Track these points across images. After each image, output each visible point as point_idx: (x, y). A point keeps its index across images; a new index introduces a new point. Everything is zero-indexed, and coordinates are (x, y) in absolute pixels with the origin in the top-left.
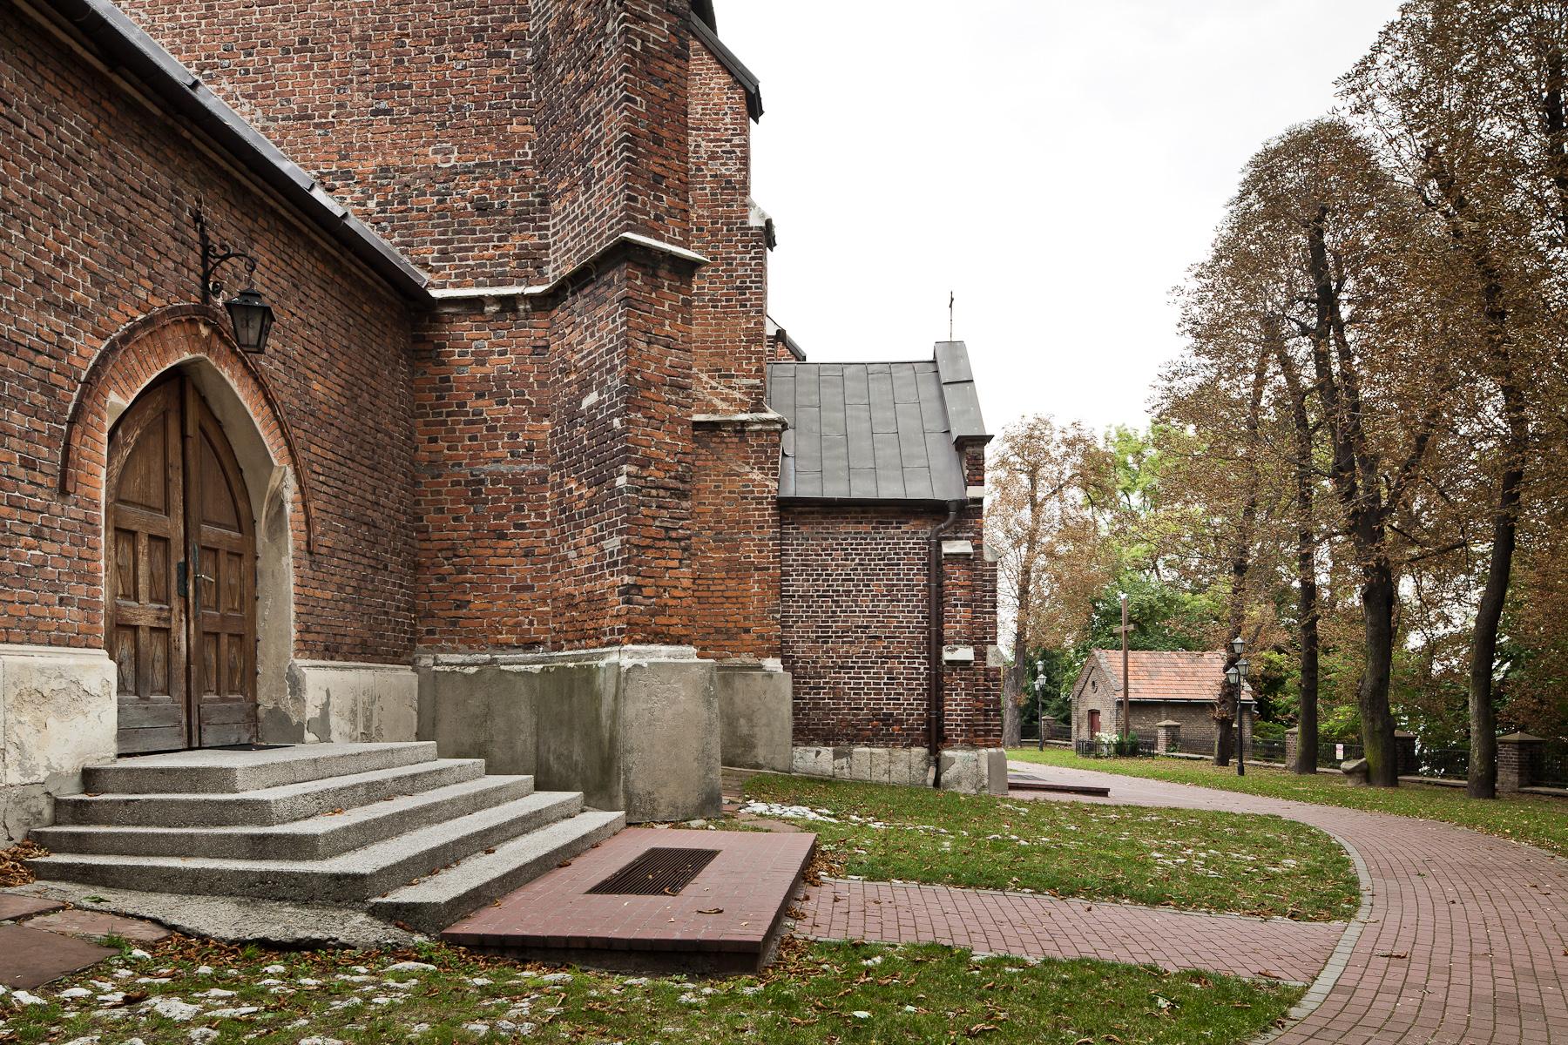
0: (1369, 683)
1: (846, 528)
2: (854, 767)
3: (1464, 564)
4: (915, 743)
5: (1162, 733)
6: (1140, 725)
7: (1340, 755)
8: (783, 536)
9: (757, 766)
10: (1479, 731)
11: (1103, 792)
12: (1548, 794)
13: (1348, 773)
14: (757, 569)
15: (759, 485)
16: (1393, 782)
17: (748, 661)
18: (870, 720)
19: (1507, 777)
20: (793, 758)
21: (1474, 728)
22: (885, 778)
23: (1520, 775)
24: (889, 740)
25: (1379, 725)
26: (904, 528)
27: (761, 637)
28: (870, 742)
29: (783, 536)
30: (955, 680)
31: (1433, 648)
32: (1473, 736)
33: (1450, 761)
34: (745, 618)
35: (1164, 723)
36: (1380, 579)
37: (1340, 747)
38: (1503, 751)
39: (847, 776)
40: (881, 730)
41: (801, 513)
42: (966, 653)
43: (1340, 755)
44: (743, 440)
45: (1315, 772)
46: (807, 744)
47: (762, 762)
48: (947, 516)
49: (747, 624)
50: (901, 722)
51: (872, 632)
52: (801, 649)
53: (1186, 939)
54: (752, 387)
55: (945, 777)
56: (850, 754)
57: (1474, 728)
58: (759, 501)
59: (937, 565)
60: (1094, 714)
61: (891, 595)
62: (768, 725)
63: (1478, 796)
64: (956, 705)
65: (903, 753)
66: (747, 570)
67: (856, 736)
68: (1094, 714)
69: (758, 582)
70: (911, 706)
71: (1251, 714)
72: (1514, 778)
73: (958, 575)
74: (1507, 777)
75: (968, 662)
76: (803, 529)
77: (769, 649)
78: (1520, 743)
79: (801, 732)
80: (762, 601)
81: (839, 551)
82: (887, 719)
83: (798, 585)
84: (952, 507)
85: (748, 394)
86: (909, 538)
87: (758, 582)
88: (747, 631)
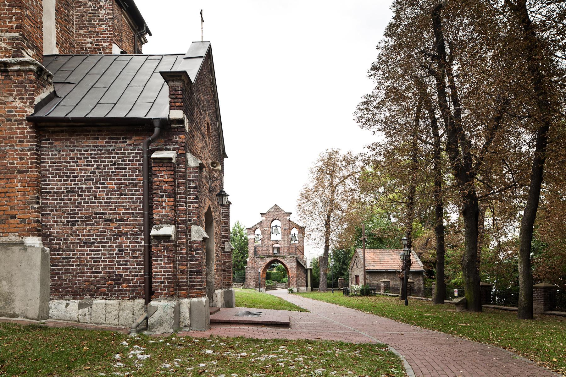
0: (466, 258)
1: (86, 144)
2: (94, 314)
3: (512, 215)
4: (137, 296)
5: (382, 284)
6: (376, 281)
7: (456, 294)
8: (39, 148)
9: (15, 315)
10: (524, 282)
11: (286, 325)
12: (559, 315)
13: (457, 304)
14: (19, 172)
15: (19, 111)
16: (479, 309)
17: (14, 239)
18: (106, 281)
19: (538, 306)
20: (48, 309)
21: (521, 280)
22: (116, 322)
23: (545, 305)
24: (119, 294)
25: (472, 279)
26: (129, 142)
27: (23, 221)
28: (106, 296)
29: (39, 148)
30: (159, 248)
31: (500, 247)
32: (521, 284)
33: (510, 297)
34: (12, 208)
35: (383, 280)
36: (471, 202)
37: (456, 290)
38: (536, 292)
39: (88, 320)
40: (113, 287)
41: (54, 132)
42: (168, 230)
43: (456, 294)
44: (8, 78)
45: (443, 303)
46: (61, 298)
47: (17, 311)
48: (153, 131)
49: (13, 212)
50: (128, 281)
51: (107, 217)
52: (56, 230)
53: (426, 353)
54: (13, 39)
55: (152, 320)
56: (90, 305)
57: (521, 280)
58: (20, 122)
59: (150, 166)
60: (357, 276)
61: (120, 190)
62: (23, 285)
63: (524, 317)
64: (161, 268)
65: (128, 304)
66: (12, 173)
67: (96, 292)
68: (357, 276)
69: (20, 181)
70: (133, 269)
71: (423, 276)
72: (541, 307)
73: (164, 174)
74: (538, 306)
75: (170, 236)
76: (56, 143)
77: (29, 230)
78: (545, 288)
79: (57, 289)
80: (24, 195)
81: (79, 160)
82: (118, 280)
83: (53, 184)
84: (157, 123)
85: (11, 44)
86: (130, 149)
87: (20, 181)
88: (13, 217)
